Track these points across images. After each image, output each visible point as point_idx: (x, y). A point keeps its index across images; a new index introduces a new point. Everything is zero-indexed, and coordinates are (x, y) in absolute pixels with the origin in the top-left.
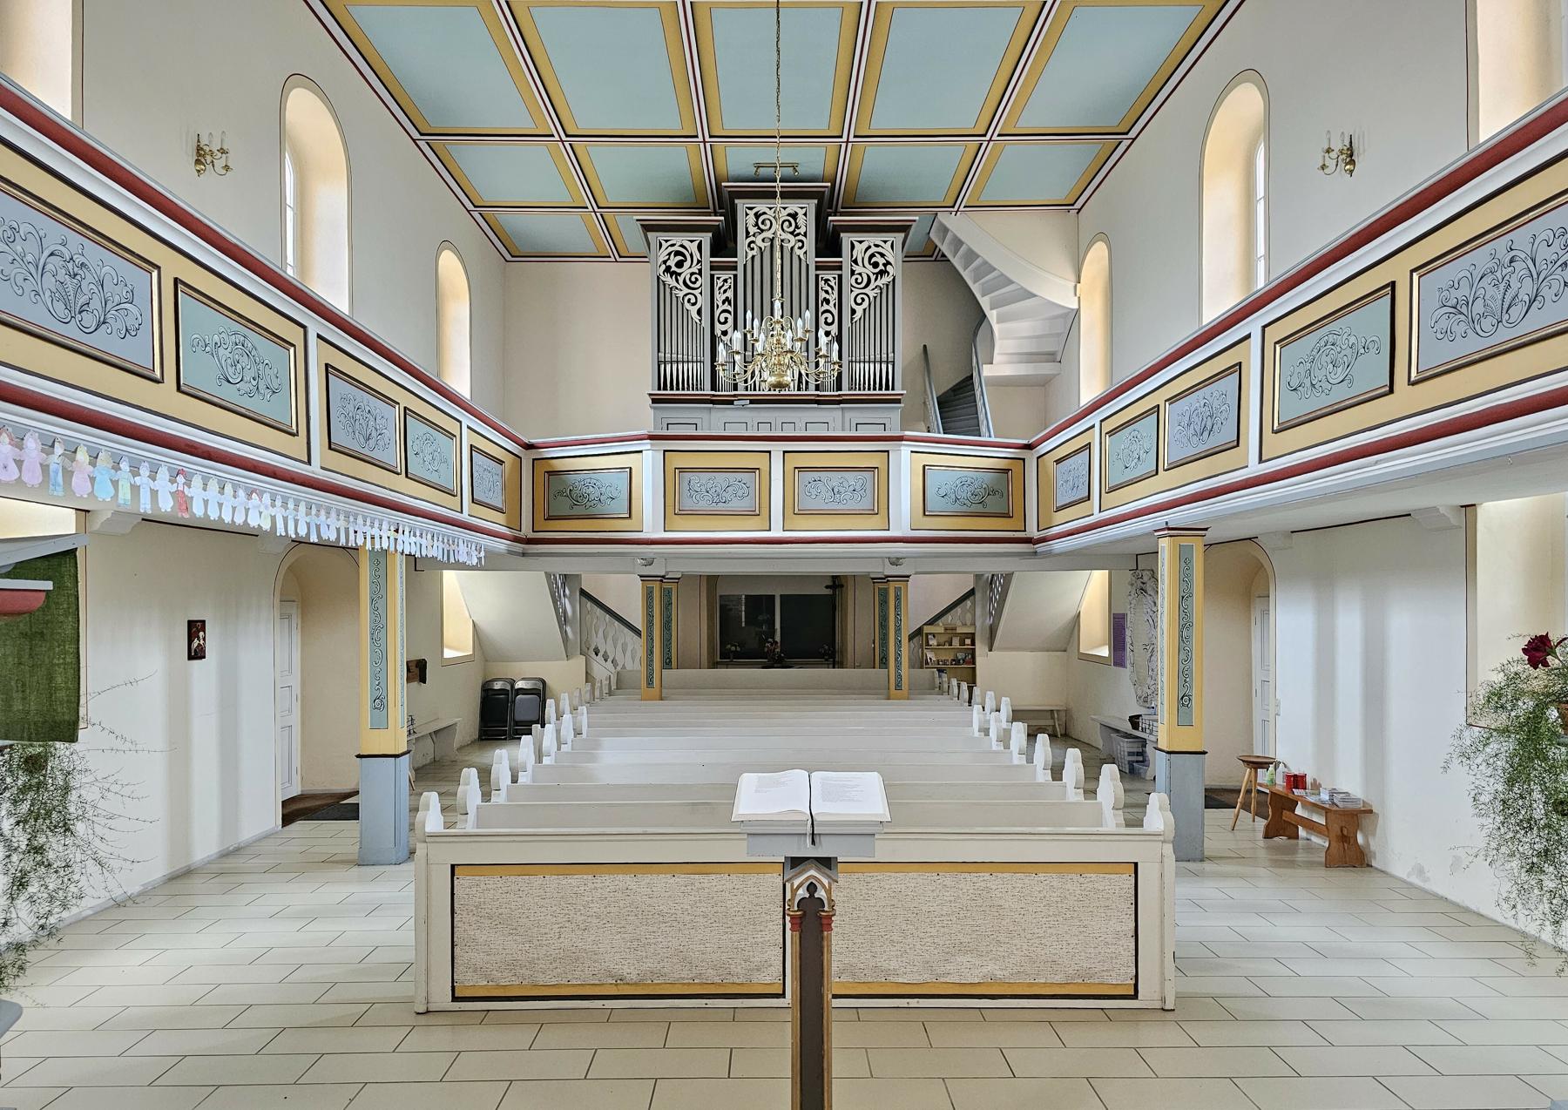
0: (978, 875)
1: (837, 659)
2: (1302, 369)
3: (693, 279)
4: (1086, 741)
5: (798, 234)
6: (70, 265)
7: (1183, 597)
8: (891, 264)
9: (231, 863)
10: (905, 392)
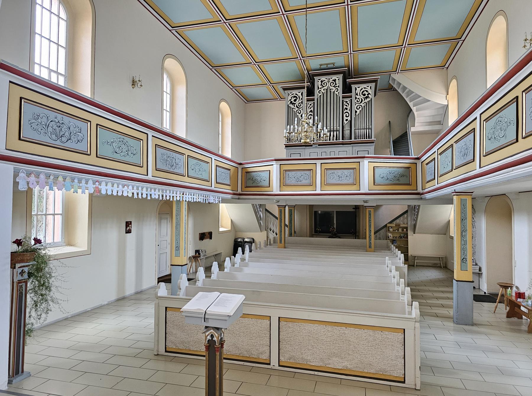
0: (341, 327)
1: (357, 235)
2: (492, 131)
3: (300, 105)
4: (449, 268)
5: (336, 87)
6: (58, 124)
7: (462, 219)
8: (370, 94)
9: (138, 296)
10: (375, 139)
